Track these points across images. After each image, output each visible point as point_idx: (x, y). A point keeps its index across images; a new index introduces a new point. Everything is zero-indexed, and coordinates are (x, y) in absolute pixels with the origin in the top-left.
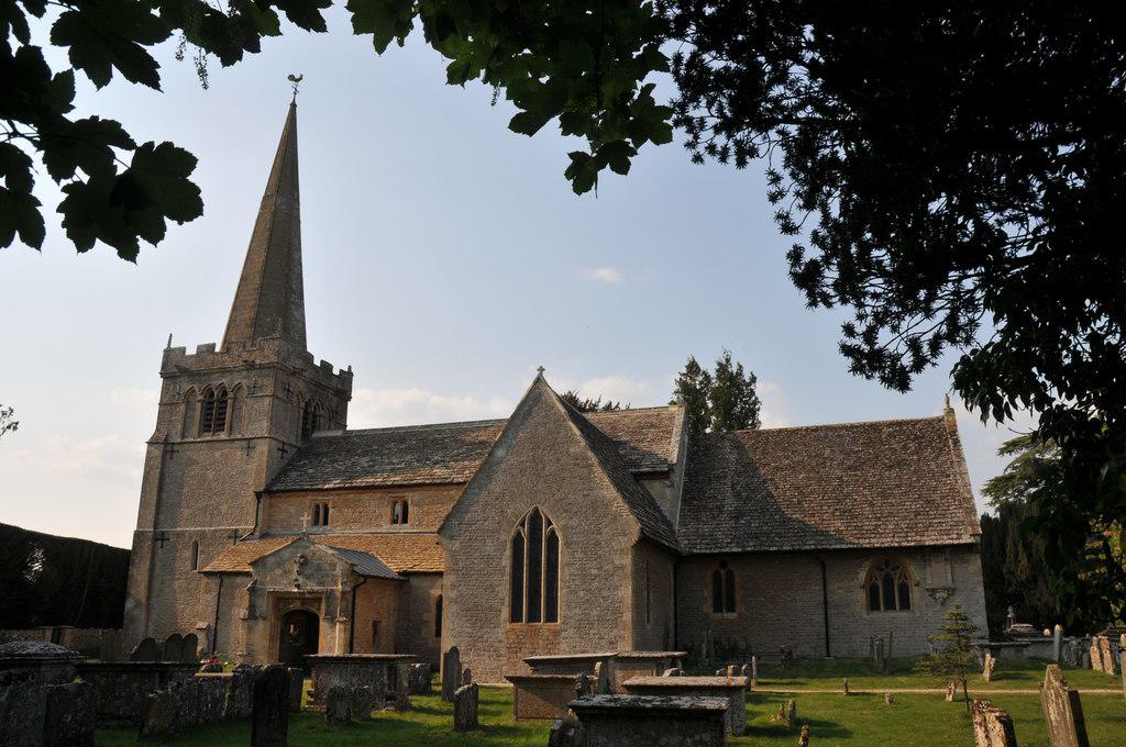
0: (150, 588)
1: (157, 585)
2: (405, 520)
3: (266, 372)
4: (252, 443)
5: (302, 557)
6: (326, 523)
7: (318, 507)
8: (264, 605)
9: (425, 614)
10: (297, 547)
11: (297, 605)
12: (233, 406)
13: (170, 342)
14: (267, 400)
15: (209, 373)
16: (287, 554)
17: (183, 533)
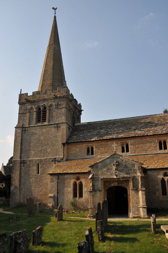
0: (20, 181)
1: (23, 180)
2: (128, 151)
3: (62, 99)
4: (59, 125)
5: (116, 162)
6: (92, 154)
7: (88, 148)
8: (100, 185)
9: (156, 186)
10: (113, 158)
11: (116, 184)
12: (49, 112)
13: (21, 92)
14: (64, 110)
15: (38, 101)
16: (108, 161)
17: (32, 160)
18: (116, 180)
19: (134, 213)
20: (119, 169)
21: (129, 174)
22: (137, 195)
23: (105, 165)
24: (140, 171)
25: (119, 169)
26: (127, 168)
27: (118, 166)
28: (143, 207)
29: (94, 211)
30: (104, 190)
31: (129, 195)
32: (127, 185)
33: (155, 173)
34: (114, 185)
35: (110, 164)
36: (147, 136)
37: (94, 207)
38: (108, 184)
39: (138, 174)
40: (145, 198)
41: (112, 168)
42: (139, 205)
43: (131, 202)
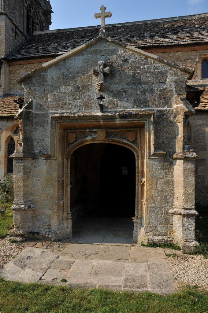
5: (105, 65)
8: (47, 138)
10: (96, 52)
11: (99, 137)
18: (102, 122)
19: (152, 229)
20: (113, 87)
21: (146, 106)
22: (166, 174)
23: (67, 77)
24: (182, 97)
25: (113, 87)
26: (140, 84)
27: (111, 78)
28: (185, 215)
29: (30, 217)
30: (63, 154)
31: (140, 174)
32: (135, 142)
33: (199, 121)
34: (93, 140)
35: (83, 71)
36: (178, 46)
37: (29, 207)
38: (76, 138)
39: (175, 106)
40: (194, 187)
41: (91, 85)
42: (172, 207)
43: (145, 194)
